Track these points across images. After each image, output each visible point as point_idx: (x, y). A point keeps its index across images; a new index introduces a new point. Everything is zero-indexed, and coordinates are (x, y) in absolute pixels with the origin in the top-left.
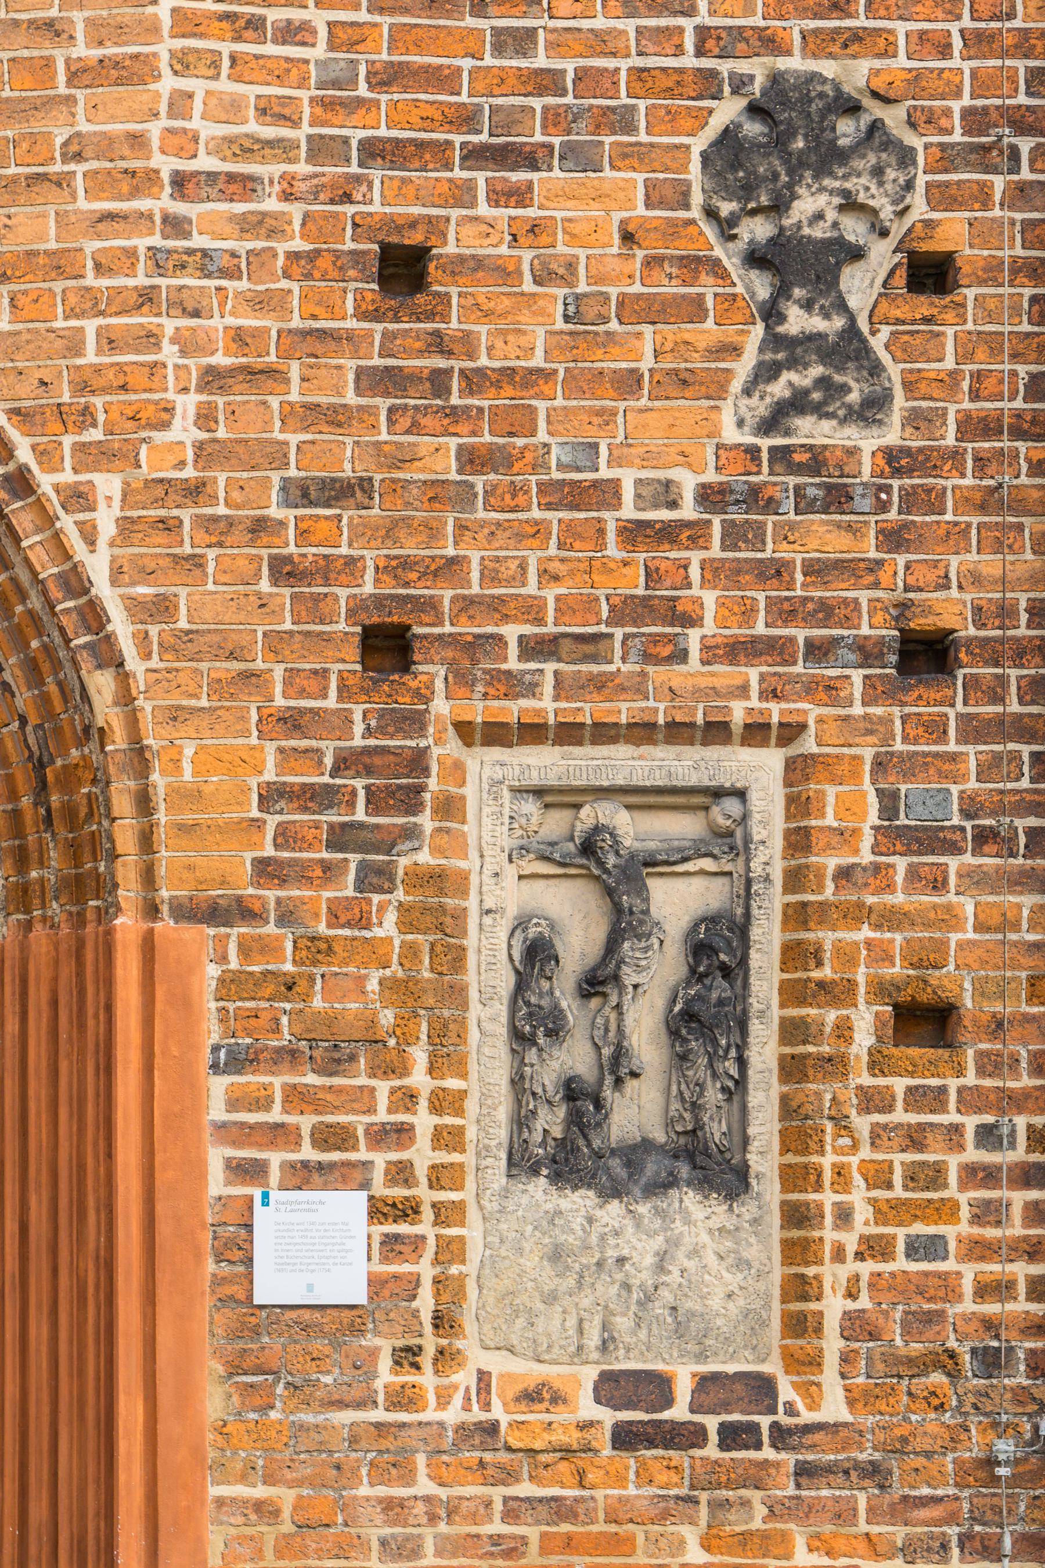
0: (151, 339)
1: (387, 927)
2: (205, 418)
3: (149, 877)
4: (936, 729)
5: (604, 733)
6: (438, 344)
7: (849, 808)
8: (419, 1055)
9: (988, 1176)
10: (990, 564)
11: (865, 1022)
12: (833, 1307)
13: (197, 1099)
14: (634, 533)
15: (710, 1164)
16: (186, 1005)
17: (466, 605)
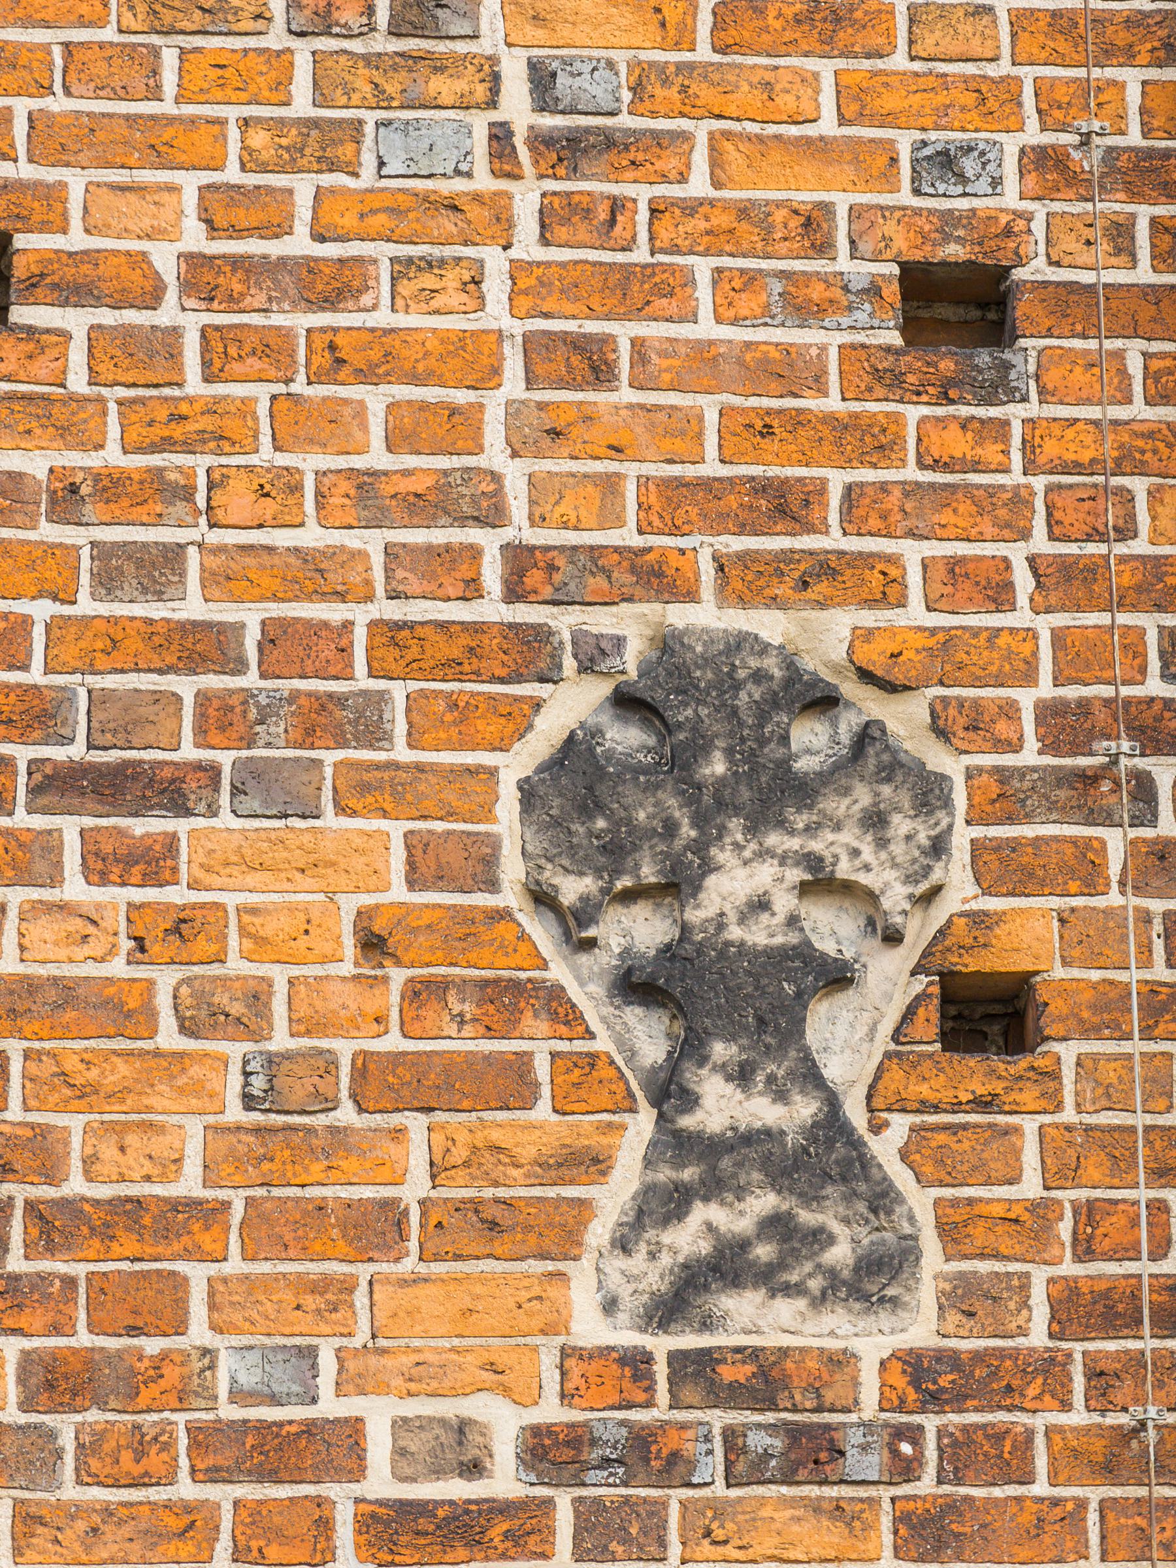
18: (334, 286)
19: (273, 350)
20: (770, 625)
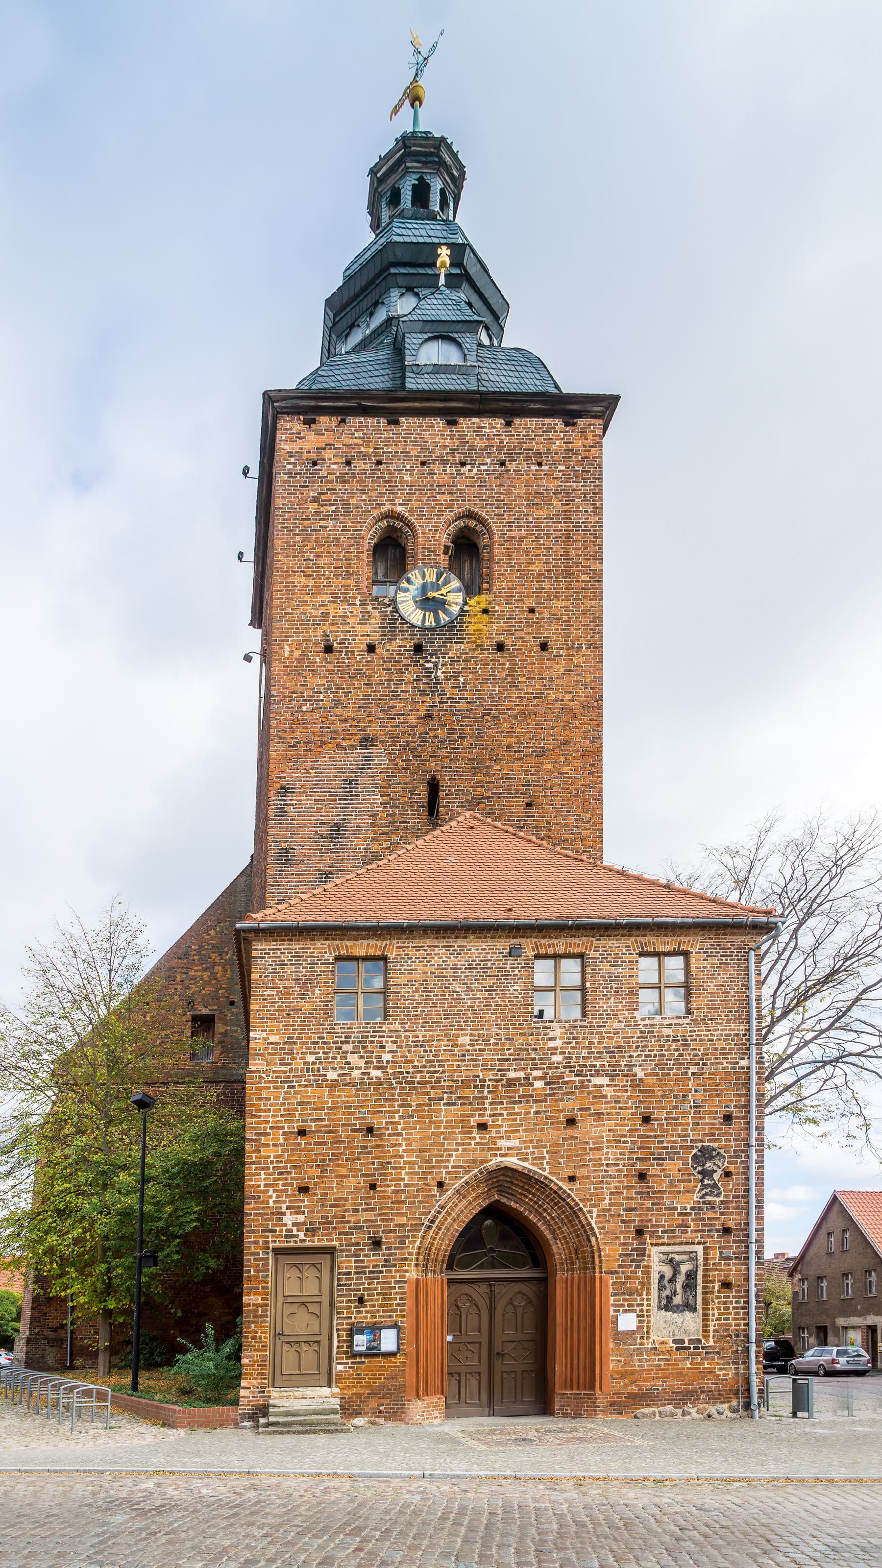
0: (602, 1188)
1: (640, 1274)
2: (610, 1199)
3: (601, 1267)
4: (729, 1242)
5: (674, 1244)
6: (648, 1187)
7: (715, 1254)
8: (644, 1293)
9: (737, 1308)
10: (738, 1217)
11: (717, 1286)
12: (711, 1328)
13: (609, 1301)
14: (680, 1214)
15: (690, 1307)
16: (607, 1286)
17: (652, 1226)
18: (677, 1119)
19: (672, 1124)
20: (711, 1144)
